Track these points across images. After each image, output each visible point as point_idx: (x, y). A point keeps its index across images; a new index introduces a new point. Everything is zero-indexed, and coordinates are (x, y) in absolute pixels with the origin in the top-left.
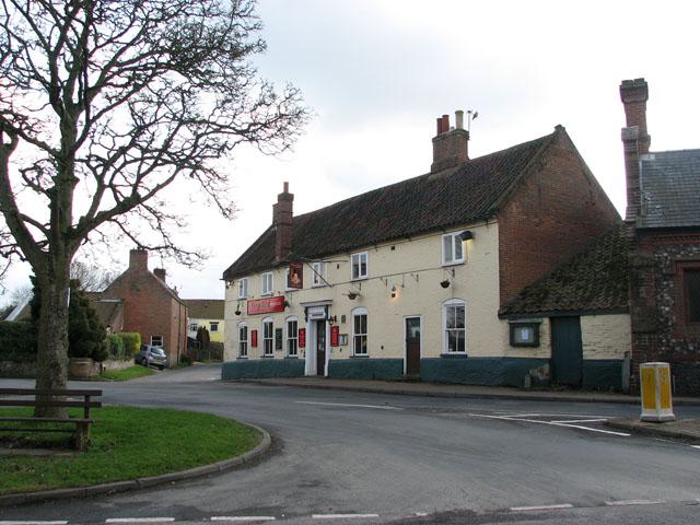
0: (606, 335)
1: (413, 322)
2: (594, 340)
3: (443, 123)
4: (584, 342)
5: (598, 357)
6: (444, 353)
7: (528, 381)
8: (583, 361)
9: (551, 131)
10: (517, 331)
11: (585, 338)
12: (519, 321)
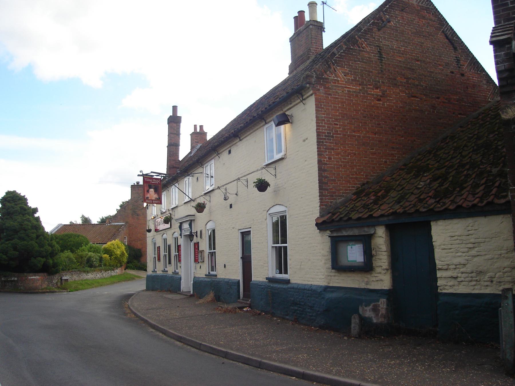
0: (473, 252)
1: (245, 235)
2: (456, 261)
3: (299, 19)
4: (439, 263)
5: (462, 289)
6: (270, 276)
7: (355, 322)
8: (438, 295)
9: (492, 46)
10: (341, 247)
11: (439, 254)
12: (345, 233)
